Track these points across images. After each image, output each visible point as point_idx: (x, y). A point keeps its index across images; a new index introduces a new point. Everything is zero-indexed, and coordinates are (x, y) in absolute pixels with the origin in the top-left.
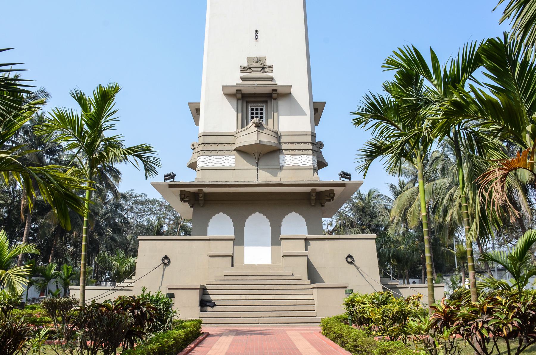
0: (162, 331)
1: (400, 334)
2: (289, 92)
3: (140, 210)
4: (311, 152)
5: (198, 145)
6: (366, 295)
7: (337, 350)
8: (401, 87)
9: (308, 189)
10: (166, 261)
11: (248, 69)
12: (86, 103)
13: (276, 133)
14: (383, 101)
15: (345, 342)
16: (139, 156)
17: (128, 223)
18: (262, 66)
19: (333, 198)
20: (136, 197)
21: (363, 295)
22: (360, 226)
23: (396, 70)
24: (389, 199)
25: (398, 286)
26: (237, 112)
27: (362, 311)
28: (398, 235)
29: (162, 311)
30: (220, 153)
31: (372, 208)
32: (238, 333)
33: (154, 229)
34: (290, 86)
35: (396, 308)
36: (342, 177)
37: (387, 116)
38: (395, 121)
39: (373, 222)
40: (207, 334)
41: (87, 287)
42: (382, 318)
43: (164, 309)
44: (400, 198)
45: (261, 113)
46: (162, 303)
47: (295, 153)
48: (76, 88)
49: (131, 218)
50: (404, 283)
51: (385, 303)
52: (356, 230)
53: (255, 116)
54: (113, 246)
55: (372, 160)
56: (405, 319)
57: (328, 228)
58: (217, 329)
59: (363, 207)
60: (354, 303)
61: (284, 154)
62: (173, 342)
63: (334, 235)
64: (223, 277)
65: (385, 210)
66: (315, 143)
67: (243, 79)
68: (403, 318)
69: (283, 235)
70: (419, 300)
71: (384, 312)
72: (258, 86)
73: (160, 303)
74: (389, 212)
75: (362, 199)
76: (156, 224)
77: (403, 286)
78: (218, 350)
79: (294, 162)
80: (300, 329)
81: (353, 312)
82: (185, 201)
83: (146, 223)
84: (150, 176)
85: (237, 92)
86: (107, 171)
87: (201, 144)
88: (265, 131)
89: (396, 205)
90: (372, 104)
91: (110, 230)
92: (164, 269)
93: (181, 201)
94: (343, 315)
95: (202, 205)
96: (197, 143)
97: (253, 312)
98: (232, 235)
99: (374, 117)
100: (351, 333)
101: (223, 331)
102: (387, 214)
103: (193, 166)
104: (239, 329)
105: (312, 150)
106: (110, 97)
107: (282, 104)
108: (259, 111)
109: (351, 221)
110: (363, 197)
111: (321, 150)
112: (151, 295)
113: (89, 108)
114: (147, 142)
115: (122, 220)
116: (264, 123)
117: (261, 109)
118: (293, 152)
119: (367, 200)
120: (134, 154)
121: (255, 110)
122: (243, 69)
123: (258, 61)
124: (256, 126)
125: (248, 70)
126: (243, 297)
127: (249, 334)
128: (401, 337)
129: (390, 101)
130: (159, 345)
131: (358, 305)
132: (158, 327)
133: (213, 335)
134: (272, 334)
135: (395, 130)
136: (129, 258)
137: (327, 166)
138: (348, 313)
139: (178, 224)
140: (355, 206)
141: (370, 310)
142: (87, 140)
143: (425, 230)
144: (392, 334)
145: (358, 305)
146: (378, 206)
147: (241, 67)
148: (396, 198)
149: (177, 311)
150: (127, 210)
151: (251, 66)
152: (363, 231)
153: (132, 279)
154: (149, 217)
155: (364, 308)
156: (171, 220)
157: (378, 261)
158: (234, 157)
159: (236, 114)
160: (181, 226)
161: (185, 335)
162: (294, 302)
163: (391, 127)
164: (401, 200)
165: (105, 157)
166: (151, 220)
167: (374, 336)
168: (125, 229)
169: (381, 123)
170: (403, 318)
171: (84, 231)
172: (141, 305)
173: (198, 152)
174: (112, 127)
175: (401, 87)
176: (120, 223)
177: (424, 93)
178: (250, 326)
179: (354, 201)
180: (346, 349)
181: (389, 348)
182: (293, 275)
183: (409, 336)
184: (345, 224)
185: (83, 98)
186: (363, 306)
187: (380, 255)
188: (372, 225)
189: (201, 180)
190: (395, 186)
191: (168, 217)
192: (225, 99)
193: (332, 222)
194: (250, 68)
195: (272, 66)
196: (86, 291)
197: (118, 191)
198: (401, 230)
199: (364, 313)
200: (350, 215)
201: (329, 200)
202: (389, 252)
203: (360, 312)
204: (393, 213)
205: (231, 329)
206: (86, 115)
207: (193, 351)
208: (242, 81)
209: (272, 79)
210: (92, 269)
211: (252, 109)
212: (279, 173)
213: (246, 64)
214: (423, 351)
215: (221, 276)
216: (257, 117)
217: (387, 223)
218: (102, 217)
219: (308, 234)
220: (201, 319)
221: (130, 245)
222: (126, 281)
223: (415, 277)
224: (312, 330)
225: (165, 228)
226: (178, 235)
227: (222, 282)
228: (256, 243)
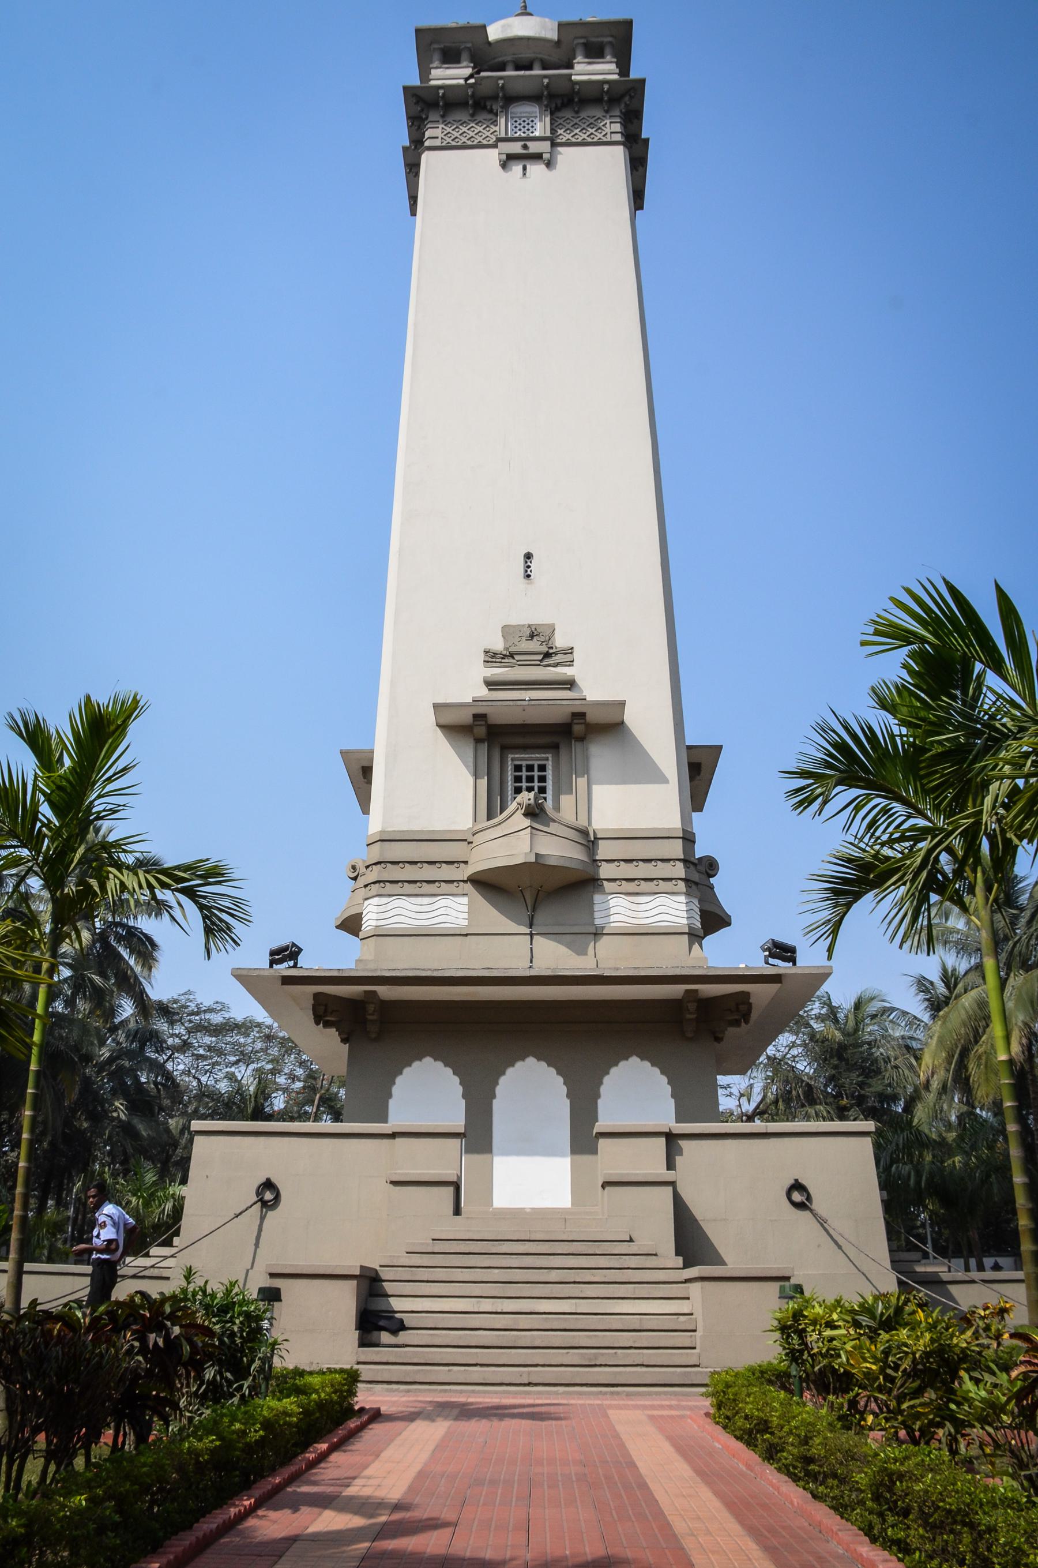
0: (236, 1400)
1: (938, 1422)
2: (618, 720)
3: (210, 1048)
4: (682, 886)
5: (367, 867)
6: (838, 1302)
7: (752, 1471)
8: (922, 695)
9: (676, 991)
10: (268, 1196)
11: (504, 657)
12: (50, 745)
13: (584, 832)
14: (872, 737)
15: (778, 1444)
16: (191, 893)
17: (175, 1085)
18: (544, 649)
19: (746, 1017)
20: (197, 1014)
21: (830, 1300)
22: (832, 1100)
23: (906, 650)
24: (914, 1021)
25: (945, 1277)
26: (476, 775)
27: (827, 1351)
28: (949, 1126)
29: (238, 1341)
30: (427, 888)
31: (866, 1046)
32: (465, 1412)
33: (245, 1103)
34: (622, 704)
35: (923, 1342)
36: (772, 955)
37: (884, 778)
38: (907, 791)
39: (870, 1086)
40: (371, 1413)
41: (28, 1266)
42: (882, 1370)
43: (245, 1334)
44: (945, 1017)
45: (542, 779)
46: (239, 1314)
48: (24, 705)
49: (183, 1073)
50: (967, 1269)
51: (889, 1324)
52: (820, 1111)
53: (524, 787)
54: (130, 1150)
55: (848, 906)
56: (955, 1375)
57: (740, 1106)
58: (404, 1399)
59: (840, 1044)
60: (803, 1326)
61: (607, 891)
62: (261, 1433)
63: (758, 1125)
64: (428, 1244)
65: (905, 1052)
66: (692, 859)
67: (491, 684)
68: (945, 1373)
70: (1003, 1318)
71: (887, 1353)
72: (533, 703)
73: (232, 1317)
74: (917, 1058)
75: (836, 1021)
76: (252, 1089)
77: (960, 1275)
78: (398, 1462)
79: (634, 915)
80: (658, 1403)
81: (801, 1352)
82: (327, 1024)
83: (223, 1086)
84: (218, 950)
85: (474, 721)
86: (119, 938)
87: (376, 864)
88: (553, 828)
89: (935, 1038)
90: (841, 747)
91: (122, 1104)
92: (263, 1218)
93: (317, 1023)
94: (776, 1362)
95: (373, 1036)
96: (364, 861)
97: (620, 1351)
99: (847, 782)
100: (794, 1417)
101: (420, 1405)
102: (911, 1065)
103: (351, 925)
104: (470, 1400)
105: (686, 880)
106: (112, 728)
108: (536, 774)
109: (808, 1084)
110: (841, 1016)
112: (209, 1291)
113: (57, 761)
114: (212, 853)
115: (157, 1078)
116: (549, 805)
117: (542, 768)
119: (851, 1023)
120: (176, 886)
121: (524, 769)
122: (492, 657)
123: (532, 636)
124: (526, 815)
125: (506, 660)
126: (487, 1305)
127: (495, 1415)
128: (940, 1432)
129: (892, 737)
130: (213, 1440)
131: (814, 1331)
132: (225, 1389)
133: (391, 1418)
134: (565, 1419)
135: (909, 817)
136: (170, 1185)
137: (729, 924)
138: (787, 1355)
139: (313, 1089)
140: (817, 1041)
141: (848, 1347)
142: (48, 847)
143: (1009, 1104)
144: (914, 1423)
145: (814, 1331)
146: (882, 1041)
147: (486, 652)
148: (934, 1017)
149: (279, 1340)
150: (175, 1049)
151: (512, 649)
152: (842, 1114)
153: (172, 1246)
154: (233, 1069)
155: (832, 1339)
156: (293, 1078)
157: (882, 1201)
158: (465, 900)
159: (471, 779)
160: (320, 1098)
161: (300, 1413)
162: (634, 1322)
163: (897, 807)
164: (948, 1024)
165: (95, 894)
166: (239, 1078)
167: (871, 1429)
168: (166, 1102)
169: (868, 798)
170: (945, 1373)
171: (29, 1100)
172: (168, 1318)
173: (366, 886)
174: (119, 811)
175: (922, 695)
176: (152, 1086)
177: (986, 713)
178: (504, 1392)
179: (815, 1026)
180: (779, 1470)
181: (902, 1469)
182: (631, 1240)
183: (968, 1430)
184: (790, 1092)
185: (42, 731)
186: (828, 1333)
187: (887, 1182)
188: (868, 1097)
189: (372, 966)
190: (932, 983)
191: (286, 1071)
193: (751, 1086)
194: (512, 655)
195: (572, 648)
196: (25, 1277)
197: (147, 995)
198: (953, 1111)
199: (832, 1356)
200: (804, 1066)
201: (736, 1023)
202: (919, 1175)
203: (820, 1353)
204: (927, 1059)
205: (439, 1400)
206: (49, 778)
207: (322, 1465)
208: (490, 690)
209: (570, 684)
210: (69, 1217)
211: (518, 768)
212: (592, 944)
214: (1009, 1479)
215: (422, 1240)
216: (530, 789)
217: (910, 1089)
218: (101, 1067)
220: (356, 1367)
221: (176, 1148)
222: (154, 1251)
223: (1001, 1252)
224: (684, 1408)
225: (276, 1102)
226: (313, 1122)
227: (426, 1260)
228: (528, 1147)
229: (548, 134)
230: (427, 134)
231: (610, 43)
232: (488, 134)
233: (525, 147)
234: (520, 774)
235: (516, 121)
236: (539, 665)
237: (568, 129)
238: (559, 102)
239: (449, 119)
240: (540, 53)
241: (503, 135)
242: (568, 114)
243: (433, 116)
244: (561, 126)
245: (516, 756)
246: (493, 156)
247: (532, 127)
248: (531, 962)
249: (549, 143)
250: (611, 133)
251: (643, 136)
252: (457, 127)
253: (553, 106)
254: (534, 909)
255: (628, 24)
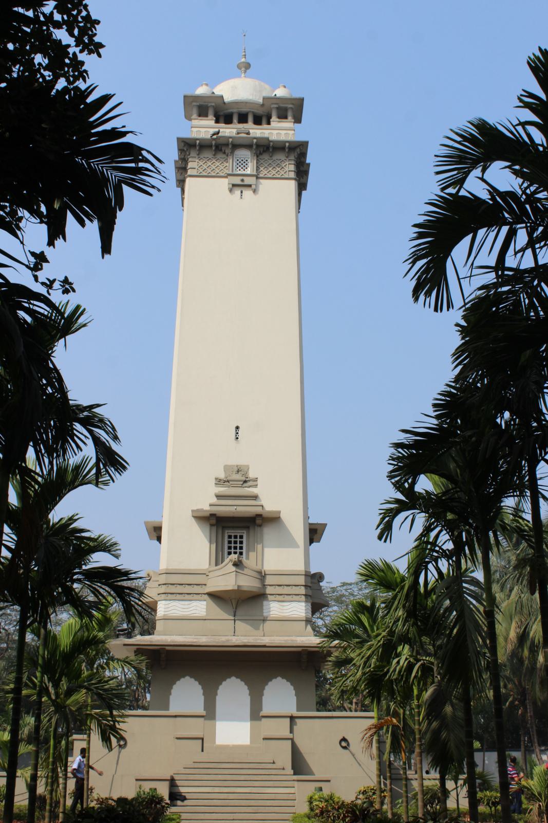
2: (278, 516)
4: (303, 597)
9: (300, 649)
13: (260, 573)
18: (244, 479)
26: (211, 542)
30: (187, 597)
34: (279, 512)
45: (241, 548)
47: (283, 599)
61: (269, 599)
67: (218, 497)
69: (265, 712)
88: (246, 571)
92: (120, 752)
97: (267, 808)
98: (202, 712)
105: (306, 595)
107: (268, 532)
108: (238, 540)
111: (321, 584)
117: (241, 537)
118: (281, 598)
121: (233, 537)
122: (219, 482)
123: (238, 471)
126: (217, 790)
147: (216, 479)
151: (229, 478)
158: (205, 603)
159: (208, 544)
162: (273, 796)
182: (274, 763)
192: (193, 518)
194: (228, 481)
195: (257, 478)
208: (218, 499)
209: (255, 497)
211: (230, 537)
212: (262, 625)
213: (222, 476)
216: (235, 553)
219: (298, 710)
229: (255, 173)
230: (190, 165)
231: (291, 108)
232: (222, 168)
233: (242, 180)
234: (236, 545)
235: (238, 160)
236: (241, 487)
237: (266, 167)
238: (262, 150)
239: (202, 157)
240: (252, 109)
241: (230, 172)
242: (266, 156)
243: (193, 153)
244: (262, 165)
245: (230, 531)
246: (225, 183)
247: (247, 164)
248: (234, 633)
249: (255, 178)
250: (289, 171)
251: (307, 161)
252: (206, 162)
253: (258, 152)
254: (236, 608)
255: (302, 100)
